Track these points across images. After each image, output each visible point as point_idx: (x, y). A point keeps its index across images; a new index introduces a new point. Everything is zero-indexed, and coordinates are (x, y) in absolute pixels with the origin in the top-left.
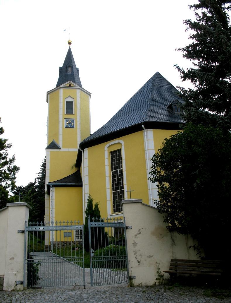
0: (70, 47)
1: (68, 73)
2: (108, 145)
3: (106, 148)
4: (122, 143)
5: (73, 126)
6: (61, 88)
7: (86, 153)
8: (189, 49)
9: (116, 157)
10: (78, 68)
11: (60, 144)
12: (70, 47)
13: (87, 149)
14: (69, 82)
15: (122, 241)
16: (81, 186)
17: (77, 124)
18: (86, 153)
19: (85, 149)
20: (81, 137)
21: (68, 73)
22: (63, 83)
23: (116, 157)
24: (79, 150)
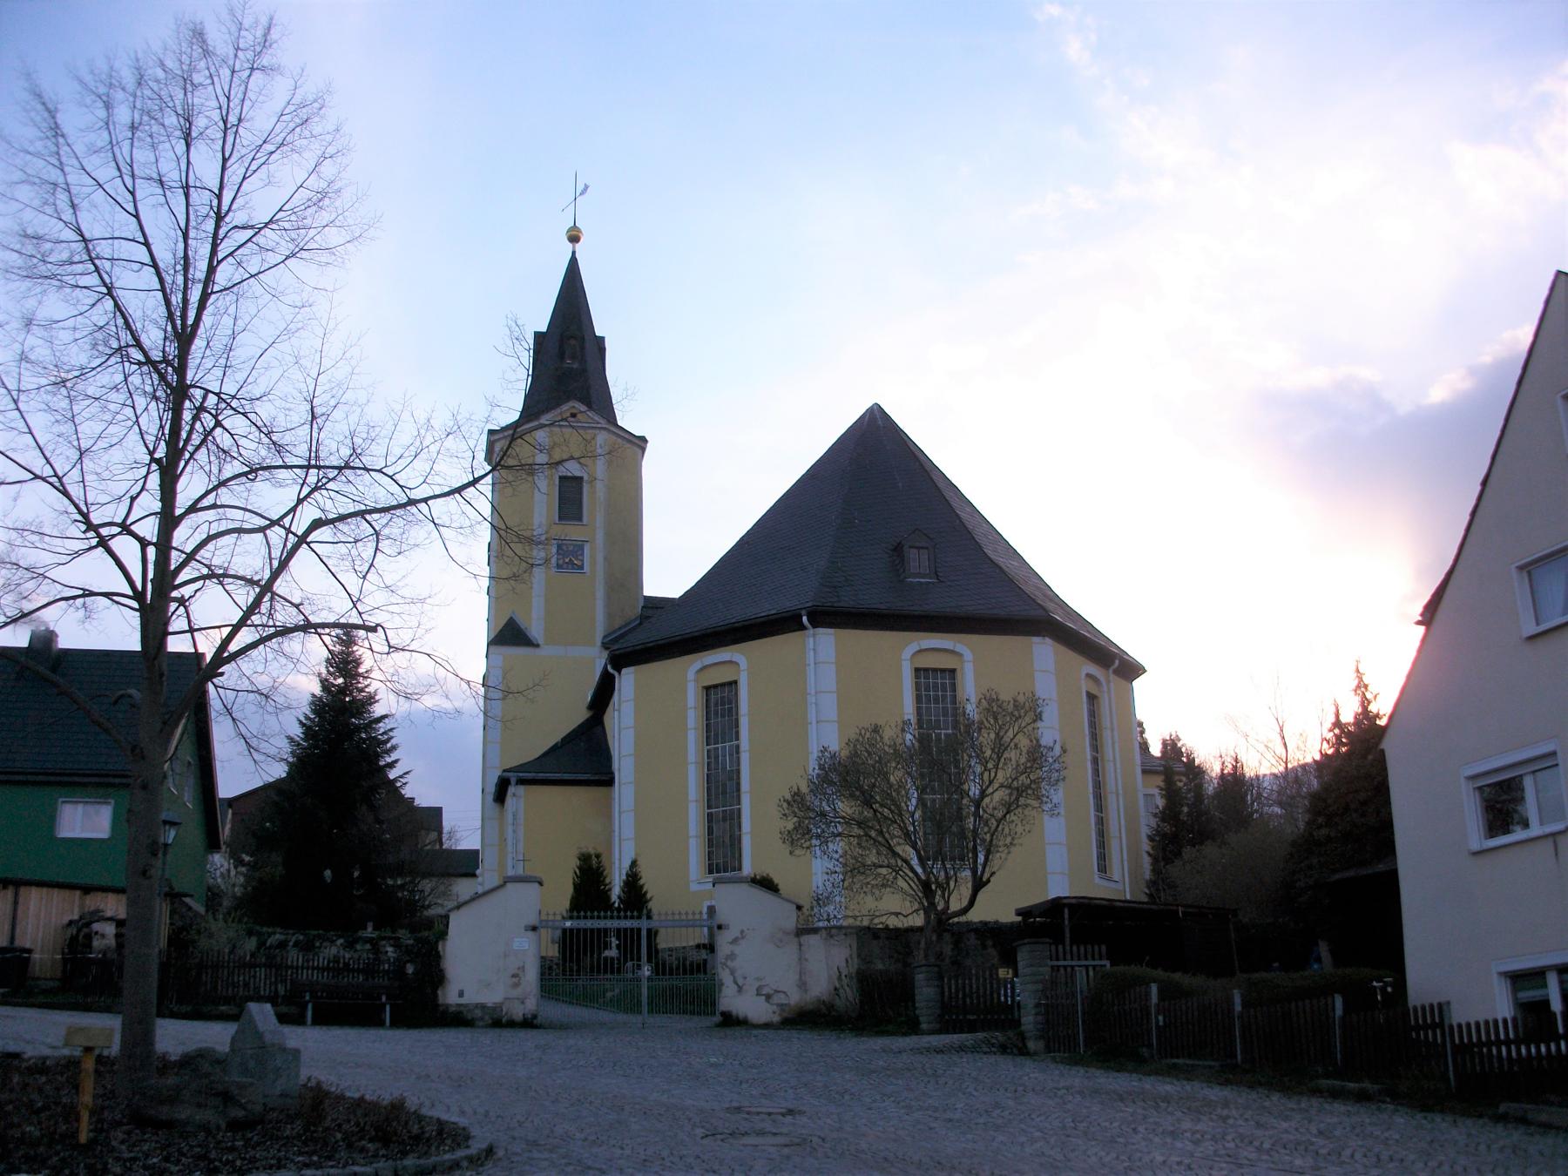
0: (574, 253)
1: (568, 360)
2: (698, 665)
3: (691, 675)
4: (741, 662)
5: (582, 567)
6: (542, 426)
7: (627, 681)
8: (607, 953)
9: (720, 703)
10: (603, 339)
11: (535, 630)
12: (574, 253)
13: (631, 669)
14: (571, 404)
15: (644, 1000)
16: (610, 782)
17: (595, 558)
18: (627, 681)
19: (624, 671)
20: (609, 616)
21: (568, 360)
22: (548, 410)
23: (720, 703)
24: (605, 668)
